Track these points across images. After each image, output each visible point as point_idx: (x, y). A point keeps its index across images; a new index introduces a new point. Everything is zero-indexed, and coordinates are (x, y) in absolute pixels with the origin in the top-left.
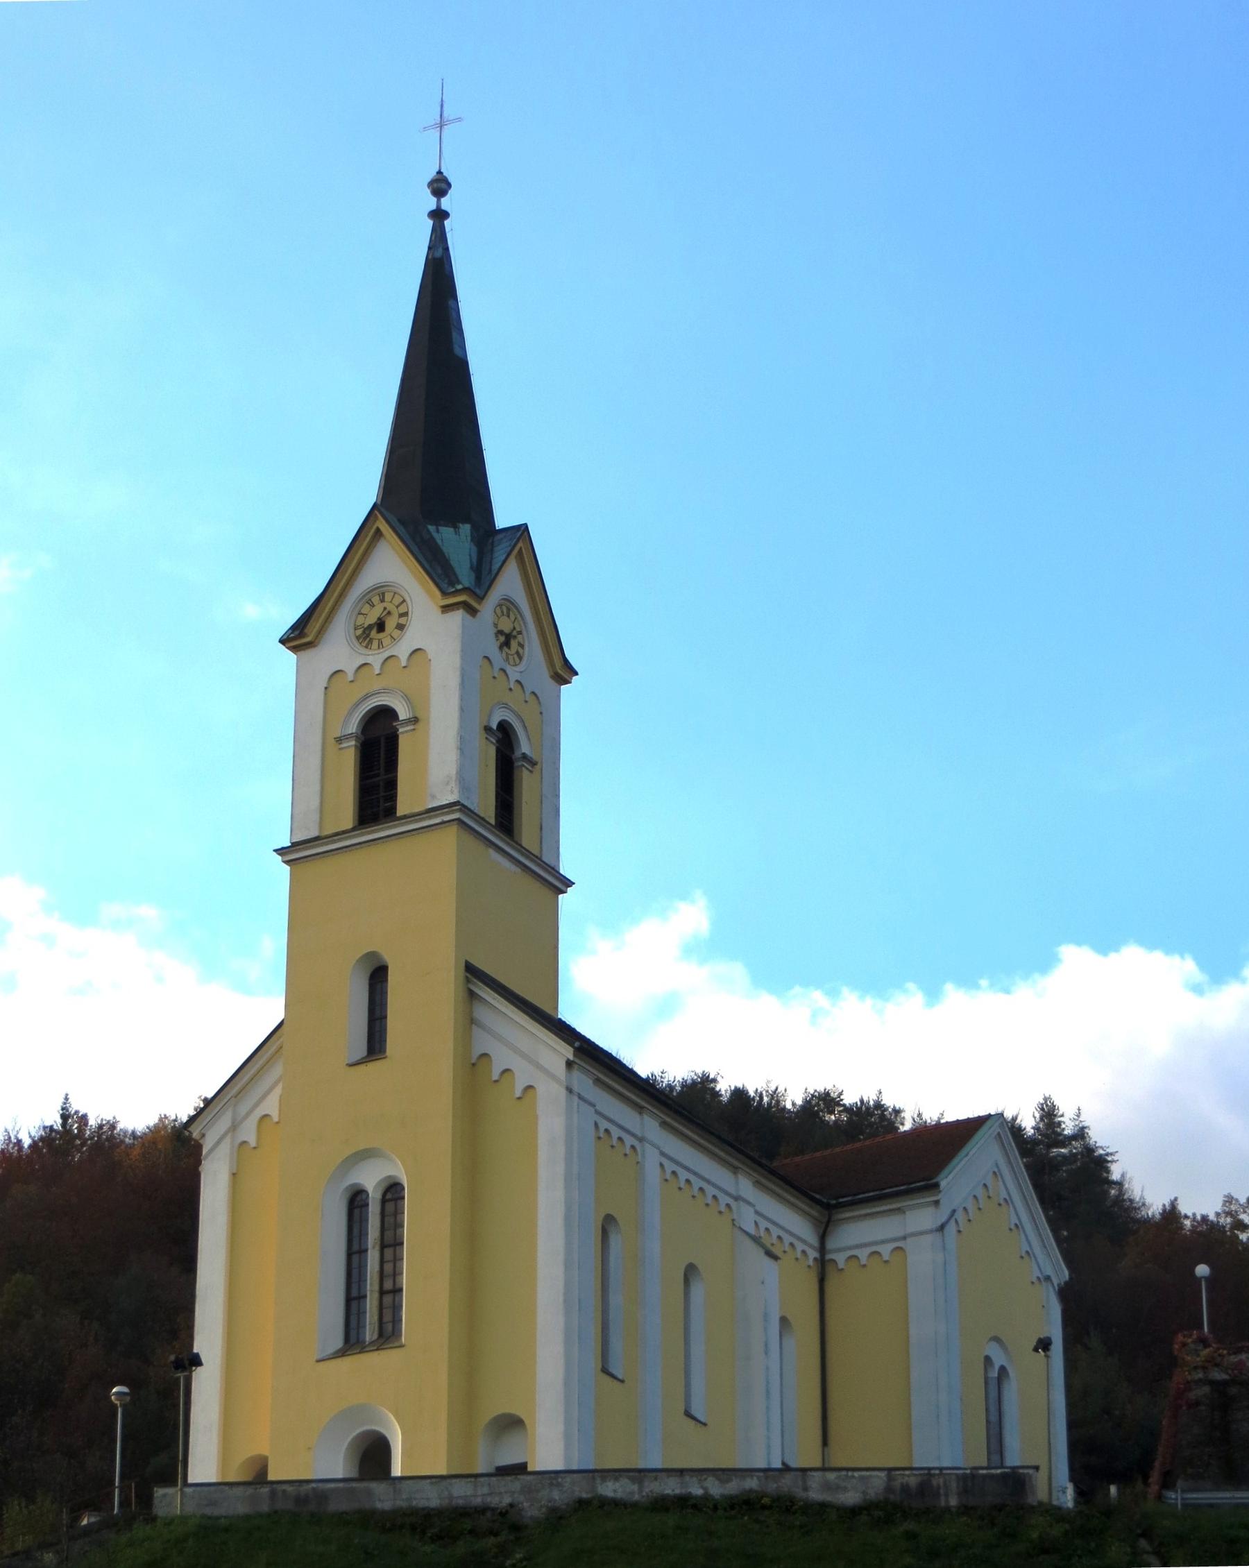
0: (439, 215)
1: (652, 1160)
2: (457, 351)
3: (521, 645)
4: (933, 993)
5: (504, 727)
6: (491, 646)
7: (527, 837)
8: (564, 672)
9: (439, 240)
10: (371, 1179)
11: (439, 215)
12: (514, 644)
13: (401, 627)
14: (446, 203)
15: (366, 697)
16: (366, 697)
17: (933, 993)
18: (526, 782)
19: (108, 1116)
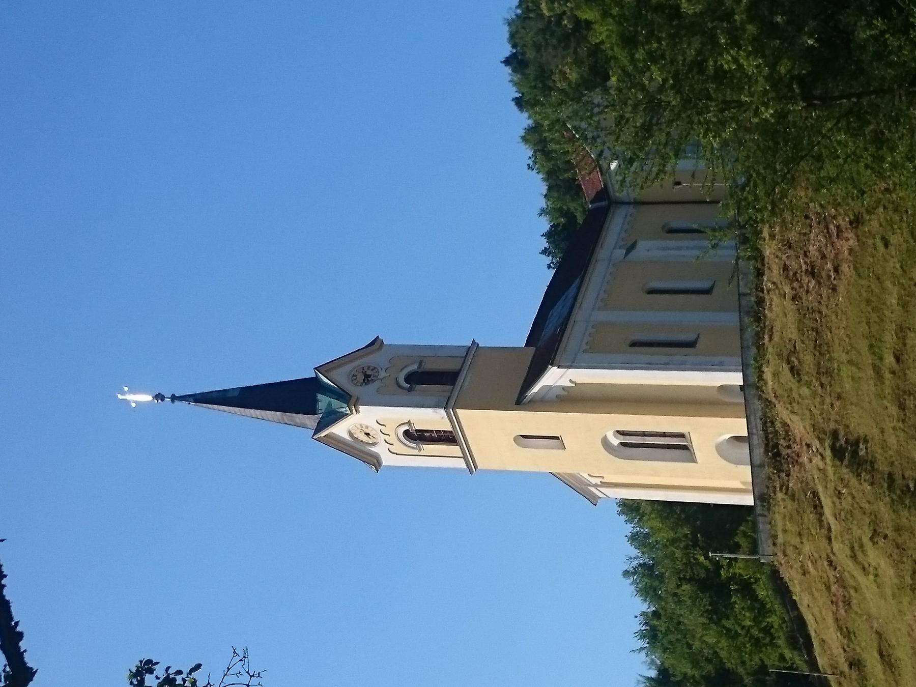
0: (174, 398)
1: (602, 316)
2: (236, 394)
3: (369, 367)
4: (20, 636)
5: (409, 378)
6: (372, 387)
7: (452, 366)
8: (376, 343)
9: (183, 398)
10: (615, 441)
11: (174, 398)
12: (369, 373)
13: (367, 427)
14: (167, 394)
15: (400, 441)
16: (400, 441)
17: (20, 636)
18: (430, 366)
19: (627, 587)
